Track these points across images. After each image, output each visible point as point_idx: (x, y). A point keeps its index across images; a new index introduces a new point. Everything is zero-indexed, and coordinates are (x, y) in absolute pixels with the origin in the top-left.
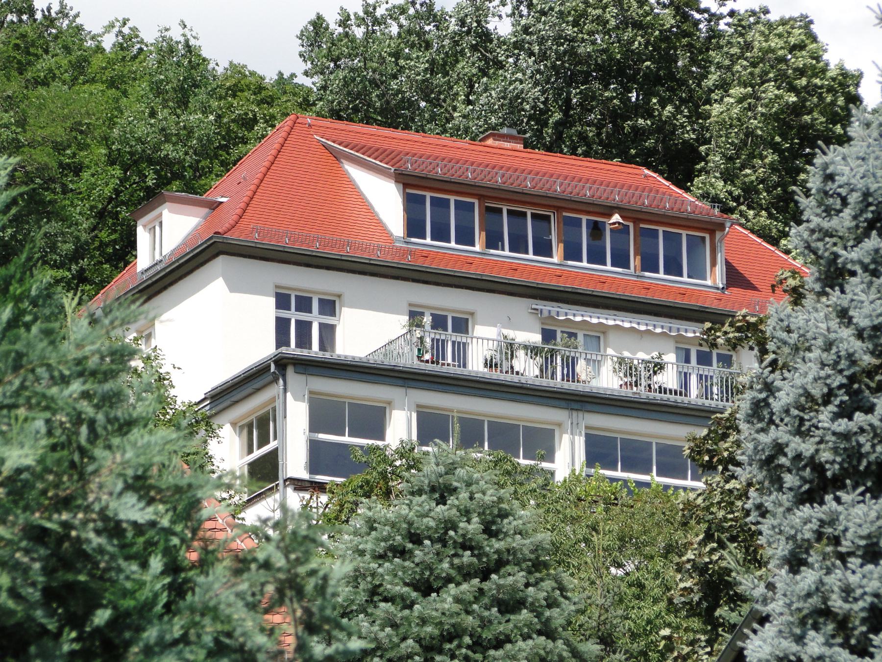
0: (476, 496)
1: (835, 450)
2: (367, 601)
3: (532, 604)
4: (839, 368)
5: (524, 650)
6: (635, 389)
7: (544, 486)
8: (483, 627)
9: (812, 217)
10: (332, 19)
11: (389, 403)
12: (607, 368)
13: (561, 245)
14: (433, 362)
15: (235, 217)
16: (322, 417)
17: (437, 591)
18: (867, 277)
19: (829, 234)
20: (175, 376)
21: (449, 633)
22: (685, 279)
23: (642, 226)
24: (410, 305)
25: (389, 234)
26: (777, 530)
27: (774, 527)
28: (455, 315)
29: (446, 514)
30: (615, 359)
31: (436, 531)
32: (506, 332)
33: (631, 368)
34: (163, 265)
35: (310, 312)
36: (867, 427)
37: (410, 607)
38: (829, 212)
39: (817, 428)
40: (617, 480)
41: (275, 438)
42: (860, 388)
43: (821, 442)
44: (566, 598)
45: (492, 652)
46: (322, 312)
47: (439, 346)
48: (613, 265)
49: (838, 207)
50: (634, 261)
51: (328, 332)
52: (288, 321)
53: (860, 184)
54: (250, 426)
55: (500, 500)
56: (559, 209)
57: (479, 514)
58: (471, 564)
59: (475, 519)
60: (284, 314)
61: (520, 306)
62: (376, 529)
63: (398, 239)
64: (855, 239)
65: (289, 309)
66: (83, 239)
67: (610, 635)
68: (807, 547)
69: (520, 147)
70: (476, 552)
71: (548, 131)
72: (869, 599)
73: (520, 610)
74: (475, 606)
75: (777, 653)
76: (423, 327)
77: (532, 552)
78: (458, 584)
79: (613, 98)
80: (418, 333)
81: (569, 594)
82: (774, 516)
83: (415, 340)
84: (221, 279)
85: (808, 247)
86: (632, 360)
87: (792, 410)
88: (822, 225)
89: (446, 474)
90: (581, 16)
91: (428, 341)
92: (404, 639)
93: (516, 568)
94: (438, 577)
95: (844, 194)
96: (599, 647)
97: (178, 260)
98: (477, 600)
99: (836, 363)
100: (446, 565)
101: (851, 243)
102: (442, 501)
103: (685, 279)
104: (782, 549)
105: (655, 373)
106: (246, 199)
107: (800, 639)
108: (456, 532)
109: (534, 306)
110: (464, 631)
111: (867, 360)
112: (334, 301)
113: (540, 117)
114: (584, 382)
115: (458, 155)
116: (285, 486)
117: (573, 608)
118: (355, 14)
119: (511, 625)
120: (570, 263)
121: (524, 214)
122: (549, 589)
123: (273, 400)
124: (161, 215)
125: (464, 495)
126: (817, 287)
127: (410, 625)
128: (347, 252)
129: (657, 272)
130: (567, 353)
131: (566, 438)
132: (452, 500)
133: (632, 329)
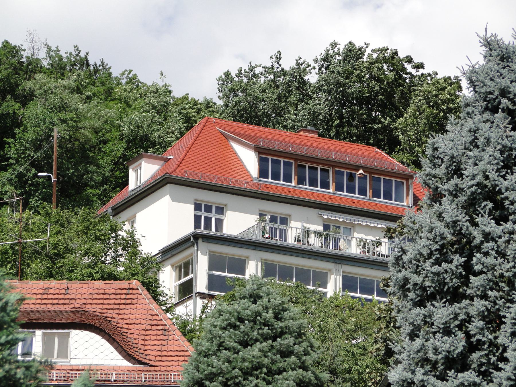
0: (271, 300)
1: (433, 281)
2: (217, 350)
3: (297, 353)
4: (436, 241)
5: (292, 376)
6: (367, 254)
7: (320, 299)
8: (272, 364)
9: (426, 168)
10: (234, 73)
11: (248, 258)
12: (354, 243)
13: (334, 184)
14: (269, 238)
15: (176, 166)
16: (215, 263)
17: (251, 345)
18: (451, 198)
19: (435, 177)
20: (142, 241)
21: (256, 366)
22: (393, 202)
23: (373, 175)
24: (260, 210)
25: (251, 176)
26: (404, 319)
27: (403, 318)
28: (206, 203)
29: (256, 309)
30: (358, 239)
31: (251, 317)
32: (305, 225)
33: (365, 244)
34: (141, 188)
35: (211, 212)
36: (449, 270)
37: (237, 353)
38: (435, 166)
39: (424, 270)
40: (356, 298)
41: (192, 273)
42: (447, 251)
43: (426, 276)
44: (314, 351)
45: (276, 376)
46: (217, 213)
47: (273, 231)
48: (359, 194)
49: (440, 164)
50: (369, 193)
51: (219, 223)
52: (201, 216)
53: (449, 153)
54: (180, 267)
55: (283, 303)
56: (333, 166)
57: (273, 309)
58: (268, 333)
59: (270, 311)
60: (199, 213)
61: (313, 212)
62: (222, 315)
63: (255, 179)
64: (447, 179)
65: (201, 211)
66: (106, 175)
67: (335, 370)
68: (418, 328)
69: (316, 136)
70: (270, 328)
71: (324, 127)
72: (444, 353)
73: (291, 356)
74: (269, 354)
75: (402, 378)
76: (266, 221)
77: (298, 328)
78: (261, 343)
79: (363, 114)
80: (263, 224)
81: (315, 349)
82: (403, 312)
83: (261, 227)
84: (168, 195)
85: (425, 183)
86: (366, 240)
87: (413, 261)
88: (431, 172)
89: (258, 289)
90: (350, 74)
91: (268, 228)
92: (234, 368)
93: (290, 336)
94: (251, 339)
95: (442, 157)
96: (329, 375)
97: (148, 186)
98: (270, 350)
99: (435, 238)
100: (255, 333)
101: (445, 181)
102: (255, 302)
103: (393, 202)
104: (407, 329)
105: (377, 247)
106: (182, 157)
107: (413, 372)
108: (261, 317)
109: (320, 213)
110: (263, 366)
111: (450, 237)
112: (223, 208)
113: (328, 121)
114: (343, 250)
115: (286, 139)
116: (196, 296)
117: (317, 356)
118: (245, 70)
119: (286, 363)
120: (338, 192)
121: (317, 168)
122: (306, 347)
123: (192, 254)
124: (141, 164)
125: (265, 300)
126: (429, 202)
127: (237, 362)
128: (230, 184)
129: (380, 198)
130: (335, 236)
131: (333, 277)
132: (259, 302)
133: (367, 225)
